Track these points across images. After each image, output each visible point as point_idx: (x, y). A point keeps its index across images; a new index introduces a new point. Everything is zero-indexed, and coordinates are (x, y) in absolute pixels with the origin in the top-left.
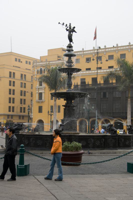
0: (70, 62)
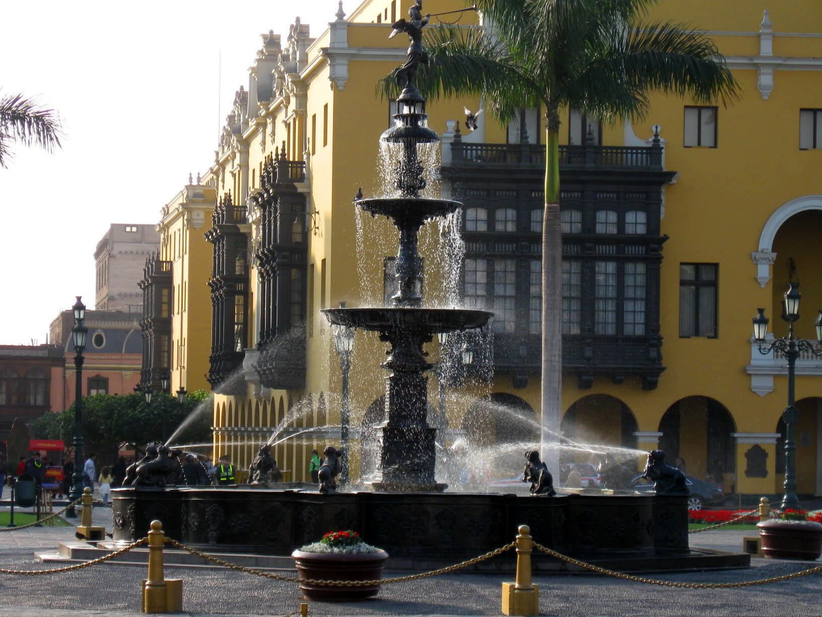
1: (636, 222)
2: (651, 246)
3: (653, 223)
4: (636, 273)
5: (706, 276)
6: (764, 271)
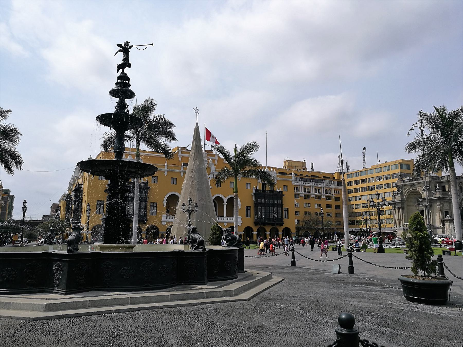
0: (122, 106)
1: (280, 202)
2: (281, 205)
3: (282, 202)
4: (280, 209)
5: (249, 208)
6: (165, 204)
